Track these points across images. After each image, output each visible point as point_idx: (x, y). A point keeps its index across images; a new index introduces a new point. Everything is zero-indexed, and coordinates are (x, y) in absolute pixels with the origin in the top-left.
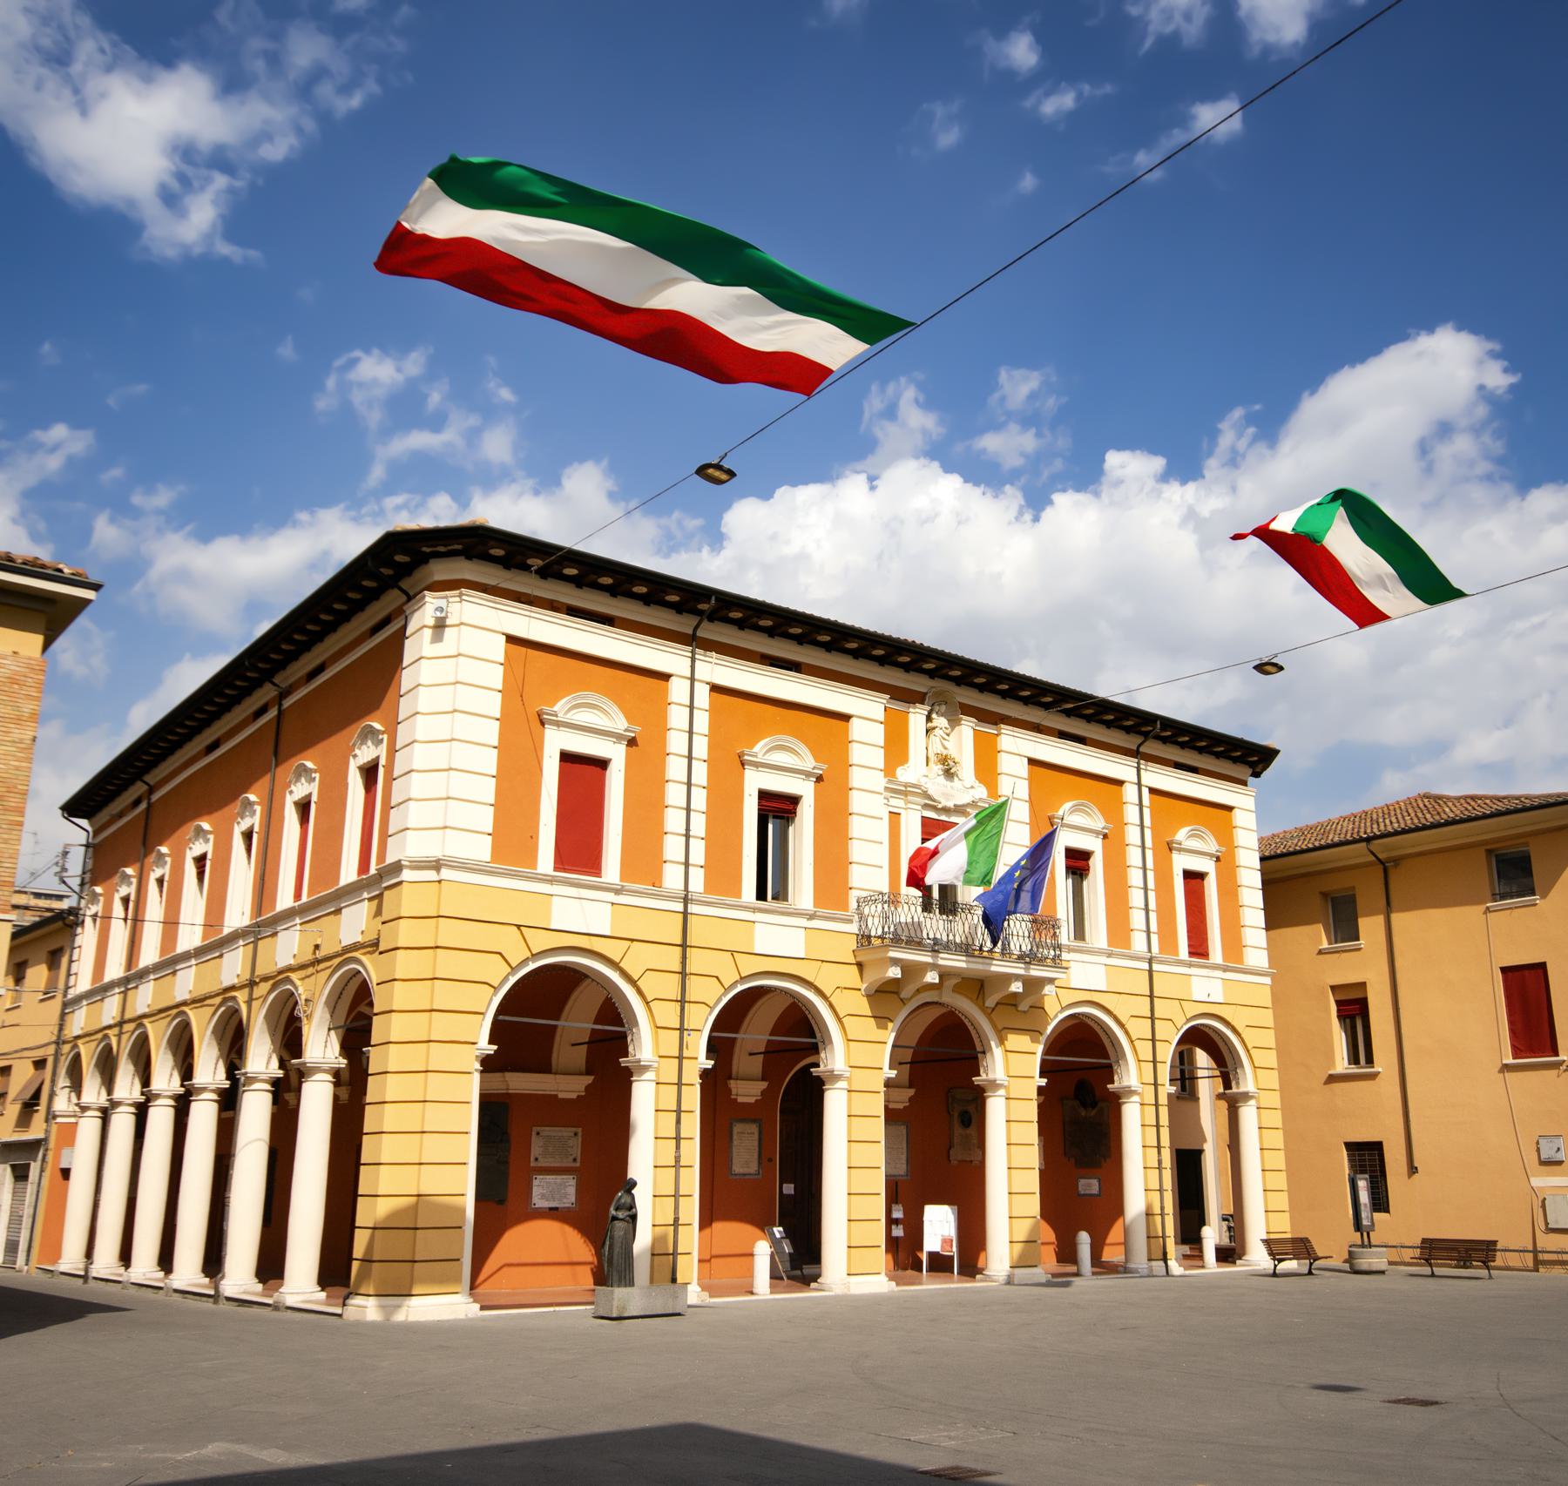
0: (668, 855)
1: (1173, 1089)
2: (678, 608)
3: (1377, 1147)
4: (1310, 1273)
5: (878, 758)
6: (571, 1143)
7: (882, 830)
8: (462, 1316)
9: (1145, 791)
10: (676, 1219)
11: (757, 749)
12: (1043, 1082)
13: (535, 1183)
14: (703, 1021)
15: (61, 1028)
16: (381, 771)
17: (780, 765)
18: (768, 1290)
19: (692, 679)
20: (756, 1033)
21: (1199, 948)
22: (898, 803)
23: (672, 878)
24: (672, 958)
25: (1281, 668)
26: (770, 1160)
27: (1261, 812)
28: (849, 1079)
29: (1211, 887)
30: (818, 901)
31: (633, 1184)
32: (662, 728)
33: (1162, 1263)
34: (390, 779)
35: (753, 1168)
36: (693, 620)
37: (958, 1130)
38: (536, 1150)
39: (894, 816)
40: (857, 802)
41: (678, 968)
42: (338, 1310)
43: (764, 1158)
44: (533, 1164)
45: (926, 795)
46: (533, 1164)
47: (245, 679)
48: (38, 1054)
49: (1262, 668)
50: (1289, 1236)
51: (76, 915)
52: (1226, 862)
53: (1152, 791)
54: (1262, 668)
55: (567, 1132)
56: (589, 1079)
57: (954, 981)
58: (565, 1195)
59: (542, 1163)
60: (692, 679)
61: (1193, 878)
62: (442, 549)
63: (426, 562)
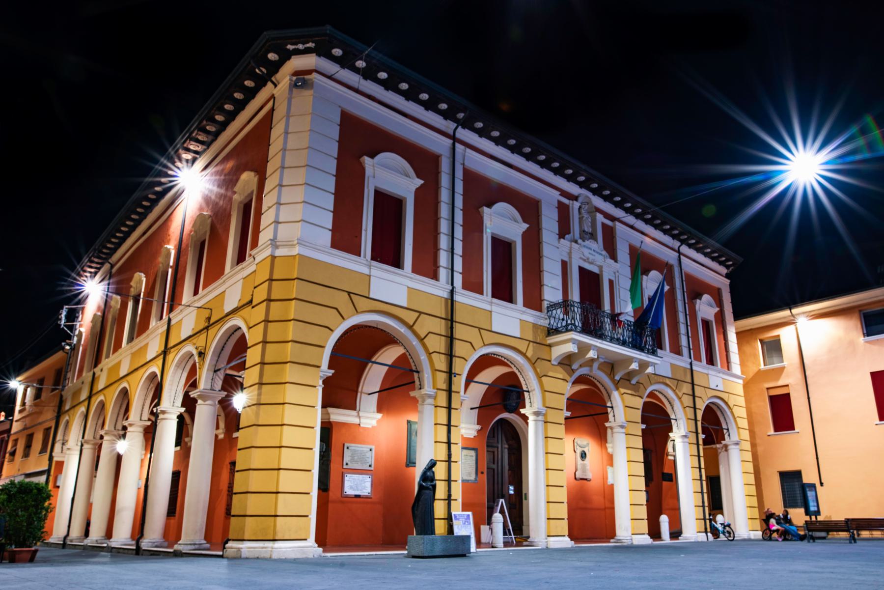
1: (704, 436)
3: (798, 474)
8: (311, 556)
12: (644, 426)
21: (711, 361)
33: (704, 534)
42: (220, 553)
44: (345, 467)
46: (345, 467)
47: (127, 226)
48: (47, 425)
58: (365, 488)
59: (350, 466)
62: (301, 47)
63: (289, 58)
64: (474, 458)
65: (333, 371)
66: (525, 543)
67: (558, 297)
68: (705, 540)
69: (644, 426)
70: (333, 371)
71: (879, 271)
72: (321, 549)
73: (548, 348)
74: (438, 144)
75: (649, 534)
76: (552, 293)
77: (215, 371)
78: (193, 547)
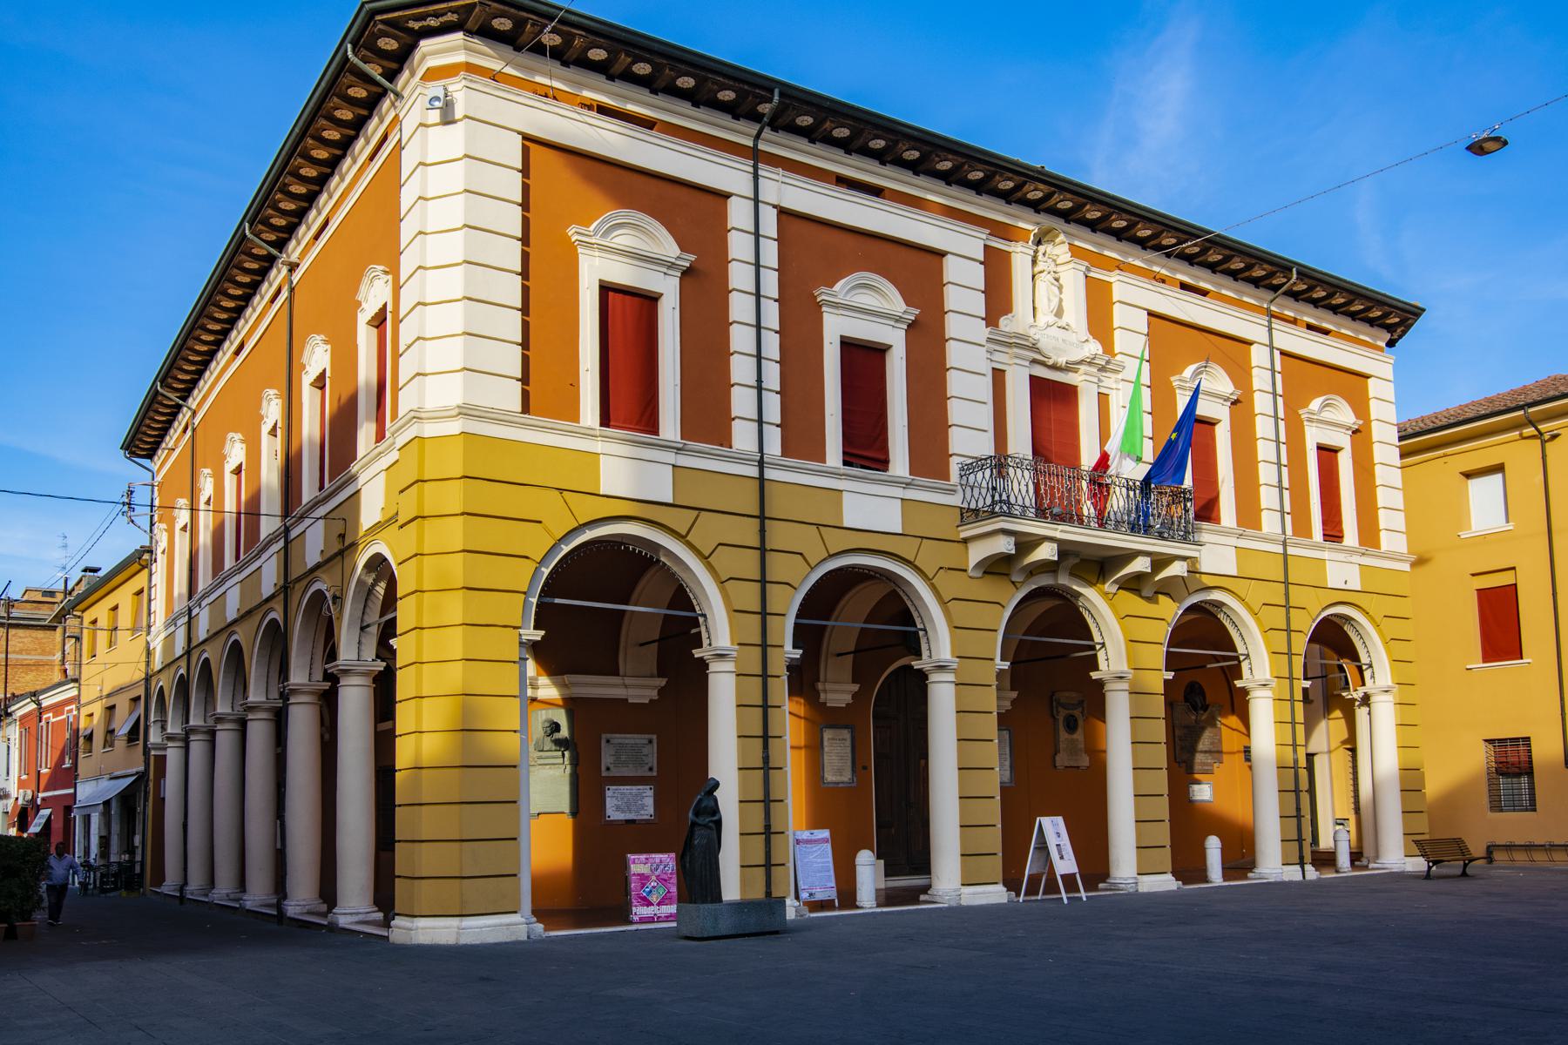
0: (734, 315)
2: (733, 110)
4: (1464, 874)
5: (978, 304)
6: (645, 751)
7: (983, 388)
9: (1277, 353)
10: (768, 827)
11: (838, 287)
12: (1170, 675)
13: (608, 793)
14: (789, 604)
15: (148, 663)
16: (389, 316)
17: (863, 309)
18: (874, 904)
19: (756, 201)
20: (847, 624)
21: (1333, 533)
22: (1003, 359)
23: (743, 437)
24: (747, 532)
25: (1505, 143)
26: (865, 768)
27: (1400, 380)
28: (955, 671)
29: (1345, 463)
30: (913, 470)
31: (716, 785)
32: (723, 261)
33: (1298, 868)
34: (397, 321)
35: (847, 776)
36: (753, 128)
37: (1063, 735)
38: (607, 759)
39: (998, 376)
40: (955, 354)
41: (756, 543)
43: (857, 765)
44: (604, 774)
45: (1034, 348)
46: (604, 774)
48: (134, 694)
49: (1478, 149)
50: (1427, 837)
51: (151, 552)
52: (1360, 435)
53: (1283, 353)
54: (1478, 149)
55: (640, 739)
56: (662, 682)
57: (1073, 561)
58: (643, 807)
59: (614, 772)
60: (756, 201)
61: (1327, 453)
64: (848, 743)
65: (542, 633)
66: (922, 897)
67: (984, 446)
68: (1299, 877)
69: (1170, 675)
70: (542, 633)
71: (639, 865)
72: (541, 926)
73: (961, 546)
74: (725, 174)
75: (1174, 873)
76: (969, 438)
77: (362, 629)
78: (356, 918)
